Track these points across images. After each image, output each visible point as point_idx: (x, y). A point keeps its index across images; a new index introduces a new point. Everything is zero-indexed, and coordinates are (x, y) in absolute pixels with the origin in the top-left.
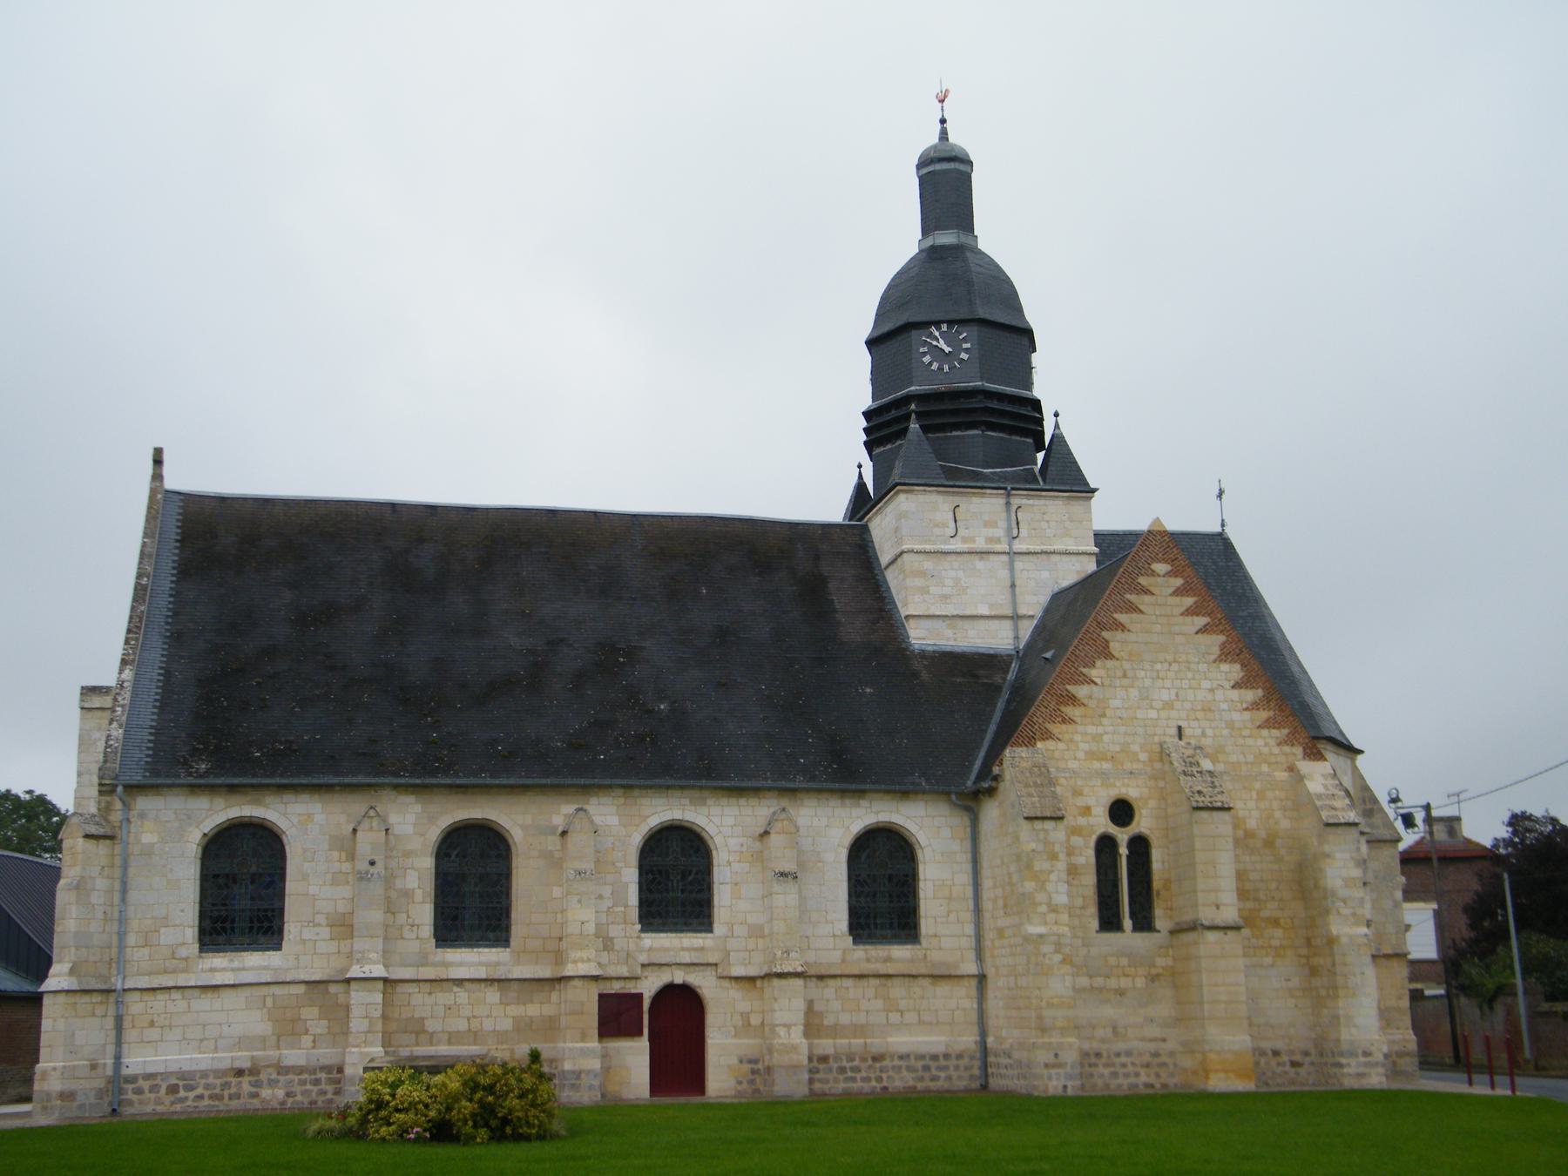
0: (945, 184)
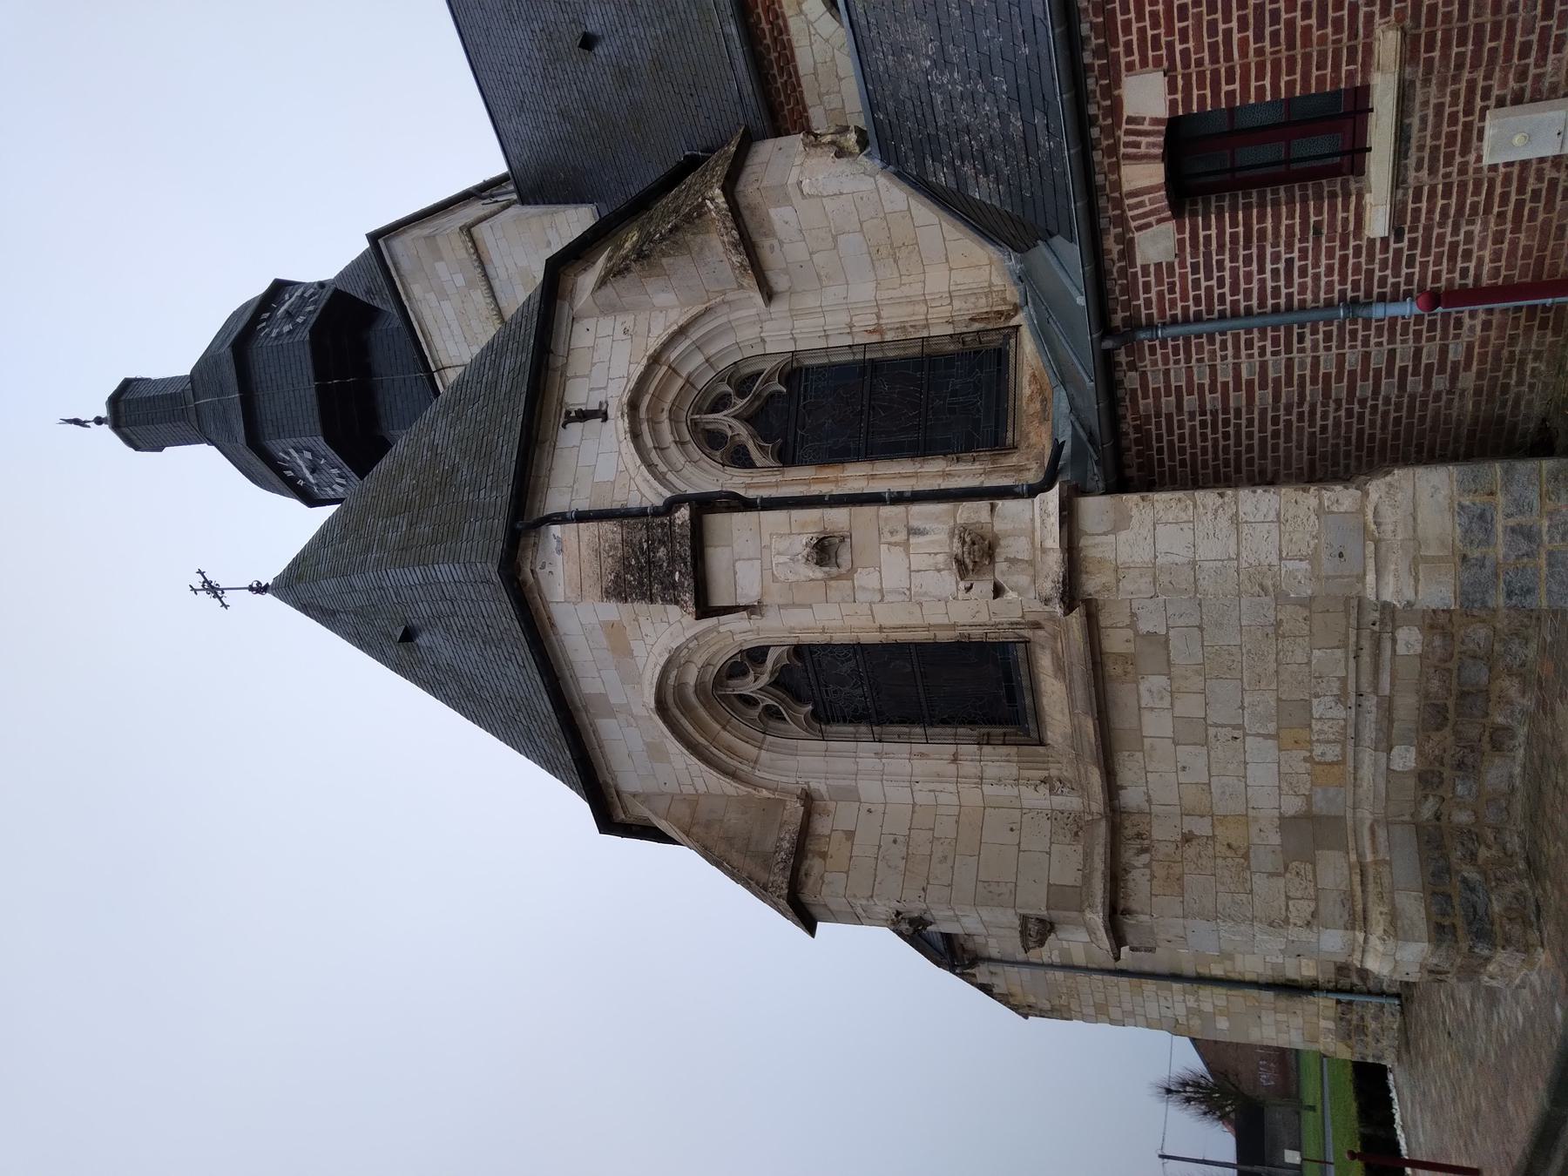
0: (143, 414)
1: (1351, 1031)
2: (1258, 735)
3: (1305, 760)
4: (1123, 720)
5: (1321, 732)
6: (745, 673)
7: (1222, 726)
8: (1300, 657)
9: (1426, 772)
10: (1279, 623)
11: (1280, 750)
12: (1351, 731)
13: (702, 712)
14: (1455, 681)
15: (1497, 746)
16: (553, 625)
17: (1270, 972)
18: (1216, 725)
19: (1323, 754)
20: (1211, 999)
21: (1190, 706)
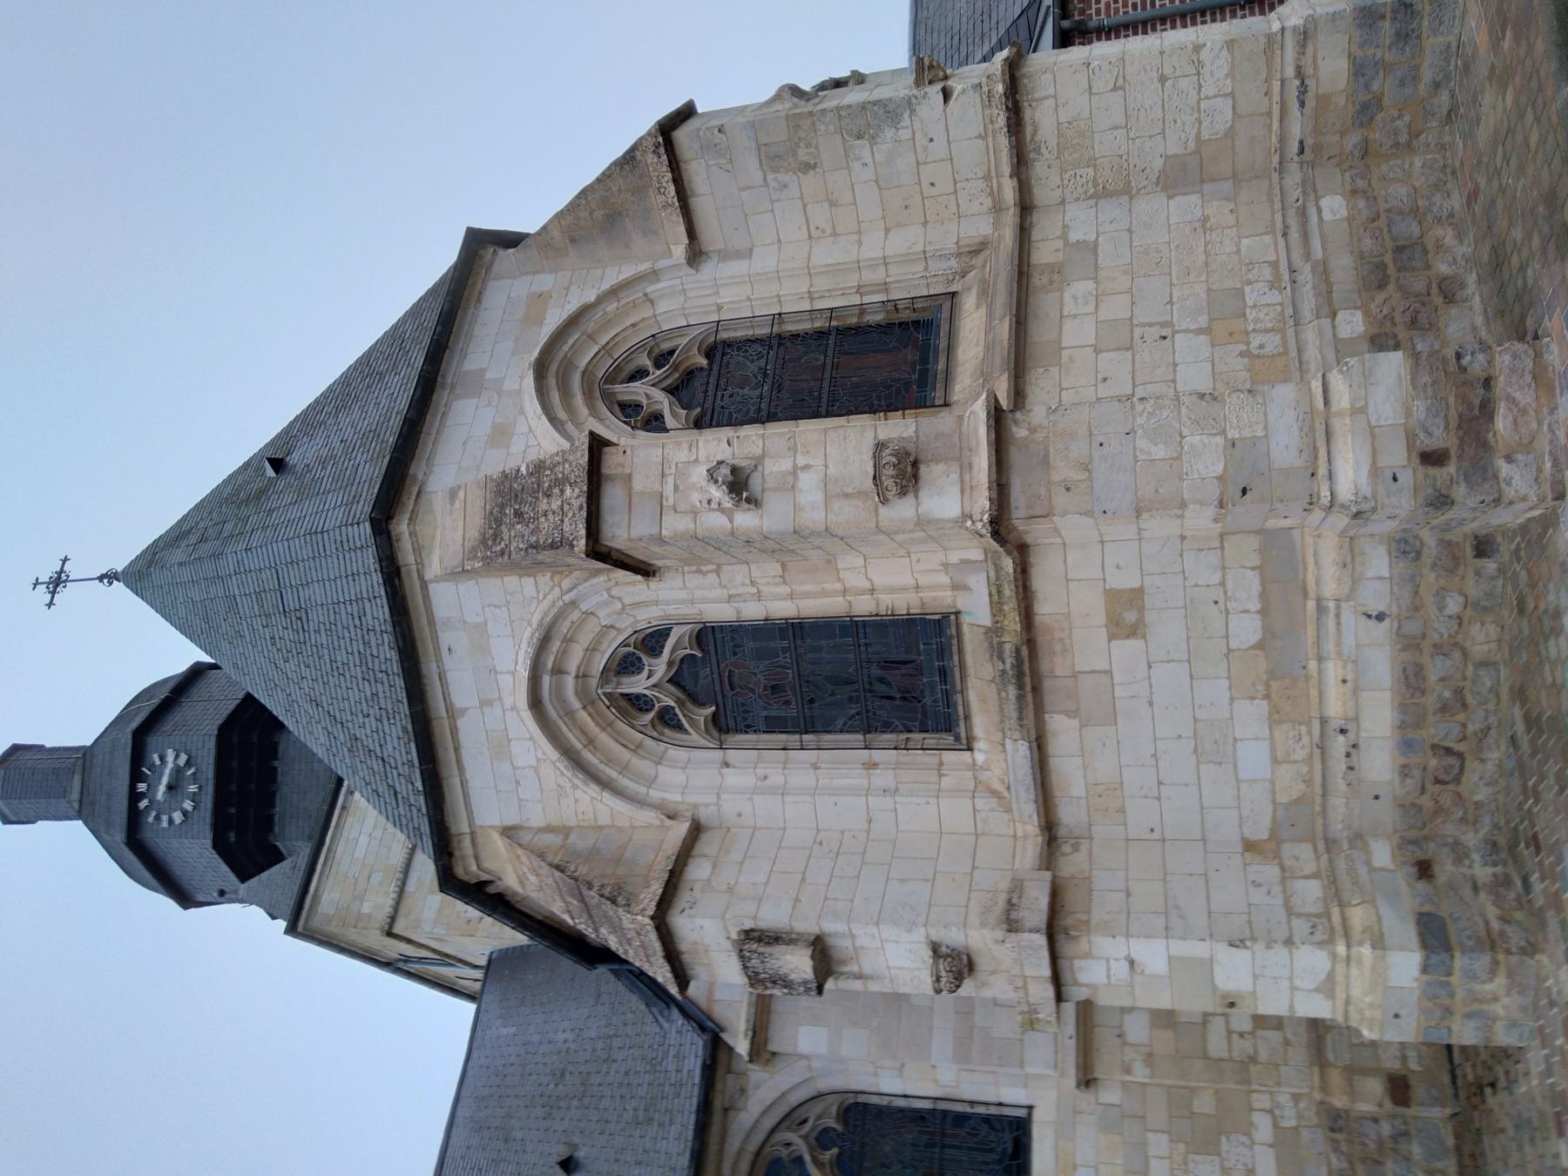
2: (1187, 331)
3: (1242, 354)
4: (1040, 333)
5: (1256, 320)
7: (1151, 325)
8: (1229, 247)
9: (1379, 335)
10: (1206, 219)
11: (1213, 346)
12: (1289, 311)
14: (1386, 236)
15: (1449, 299)
16: (479, 301)
18: (1143, 325)
19: (1261, 347)
21: (1116, 308)
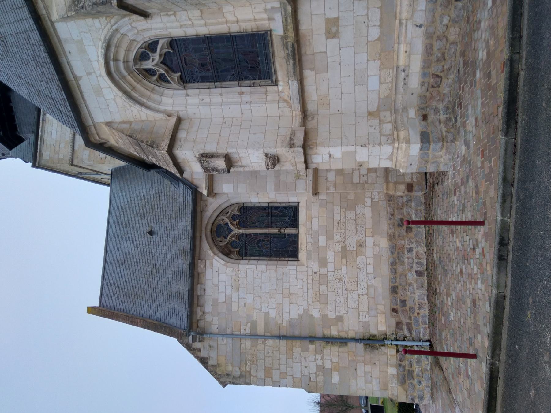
1: (406, 376)
6: (148, 58)
13: (129, 78)
17: (361, 330)
20: (331, 355)
